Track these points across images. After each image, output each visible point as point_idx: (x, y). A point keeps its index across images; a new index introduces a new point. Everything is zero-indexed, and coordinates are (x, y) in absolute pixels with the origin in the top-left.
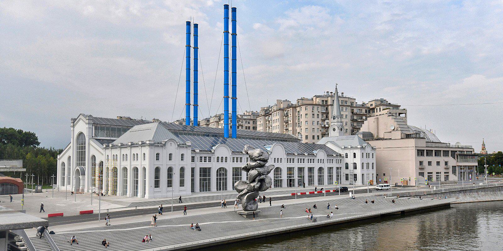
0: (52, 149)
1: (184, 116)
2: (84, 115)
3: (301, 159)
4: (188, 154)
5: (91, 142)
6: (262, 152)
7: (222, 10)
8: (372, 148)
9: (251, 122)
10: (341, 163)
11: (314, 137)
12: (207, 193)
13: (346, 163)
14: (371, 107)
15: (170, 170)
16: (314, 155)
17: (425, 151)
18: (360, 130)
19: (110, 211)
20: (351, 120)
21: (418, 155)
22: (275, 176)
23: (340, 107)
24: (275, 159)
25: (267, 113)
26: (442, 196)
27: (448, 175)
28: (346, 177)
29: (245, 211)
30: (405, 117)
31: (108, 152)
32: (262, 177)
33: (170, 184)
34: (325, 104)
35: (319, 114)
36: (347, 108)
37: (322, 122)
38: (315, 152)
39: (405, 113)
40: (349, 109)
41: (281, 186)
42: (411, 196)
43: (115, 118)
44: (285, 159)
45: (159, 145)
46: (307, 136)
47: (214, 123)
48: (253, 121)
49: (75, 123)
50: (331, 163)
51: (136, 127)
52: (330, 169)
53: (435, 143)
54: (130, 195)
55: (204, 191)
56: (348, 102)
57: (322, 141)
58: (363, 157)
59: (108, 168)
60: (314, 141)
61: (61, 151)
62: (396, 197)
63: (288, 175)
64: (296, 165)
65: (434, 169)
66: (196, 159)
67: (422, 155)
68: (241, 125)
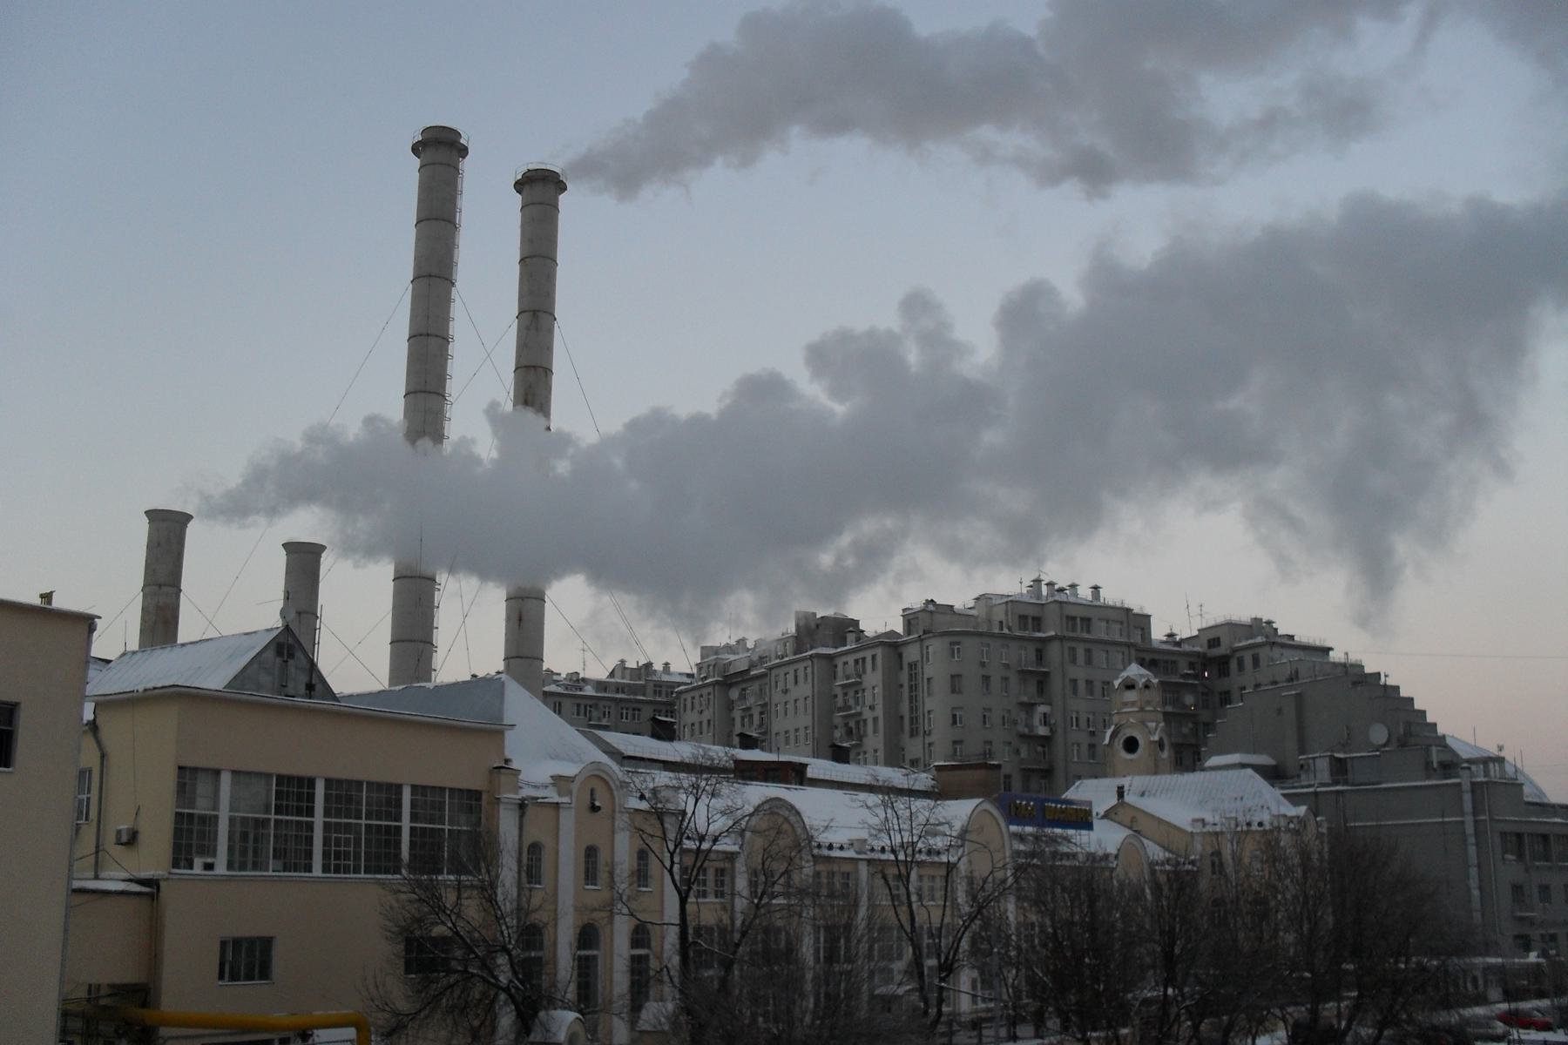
36: (988, 645)
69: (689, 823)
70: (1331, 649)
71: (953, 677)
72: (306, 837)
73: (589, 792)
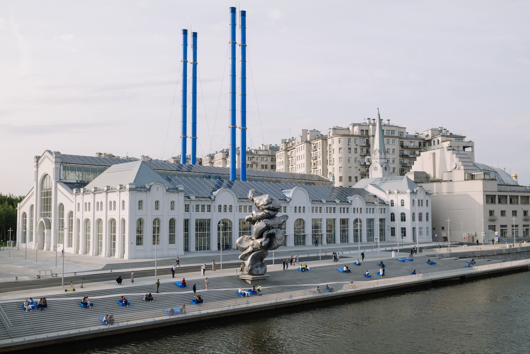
0: (11, 195)
1: (179, 152)
2: (50, 152)
3: (344, 208)
4: (179, 199)
5: (60, 187)
6: (271, 199)
7: (229, 15)
8: (426, 193)
9: (269, 159)
10: (384, 213)
11: (350, 178)
12: (204, 252)
13: (392, 213)
14: (427, 139)
15: (172, 222)
16: (348, 202)
17: (497, 197)
18: (411, 169)
19: (78, 274)
20: (400, 156)
21: (487, 202)
22: (342, 229)
23: (384, 138)
24: (296, 207)
25: (289, 146)
26: (518, 257)
27: (528, 229)
28: (392, 231)
30: (472, 152)
31: (79, 198)
32: (271, 231)
33: (155, 239)
34: (365, 135)
35: (357, 149)
38: (349, 198)
39: (472, 147)
40: (397, 140)
41: (304, 244)
42: (476, 256)
43: (95, 155)
44: (309, 208)
45: (142, 189)
46: (342, 177)
47: (220, 161)
48: (272, 157)
49: (39, 161)
50: (372, 213)
51: (114, 167)
53: (510, 185)
54: (105, 254)
55: (301, 245)
56: (395, 132)
57: (358, 186)
58: (413, 205)
59: (79, 220)
60: (350, 184)
61: (21, 199)
62: (455, 258)
63: (314, 230)
64: (324, 216)
65: (510, 220)
66: (191, 208)
67: (493, 202)
68: (254, 163)
69: (18, 243)
70: (465, 137)
71: (340, 177)
72: (241, 230)
73: (125, 209)
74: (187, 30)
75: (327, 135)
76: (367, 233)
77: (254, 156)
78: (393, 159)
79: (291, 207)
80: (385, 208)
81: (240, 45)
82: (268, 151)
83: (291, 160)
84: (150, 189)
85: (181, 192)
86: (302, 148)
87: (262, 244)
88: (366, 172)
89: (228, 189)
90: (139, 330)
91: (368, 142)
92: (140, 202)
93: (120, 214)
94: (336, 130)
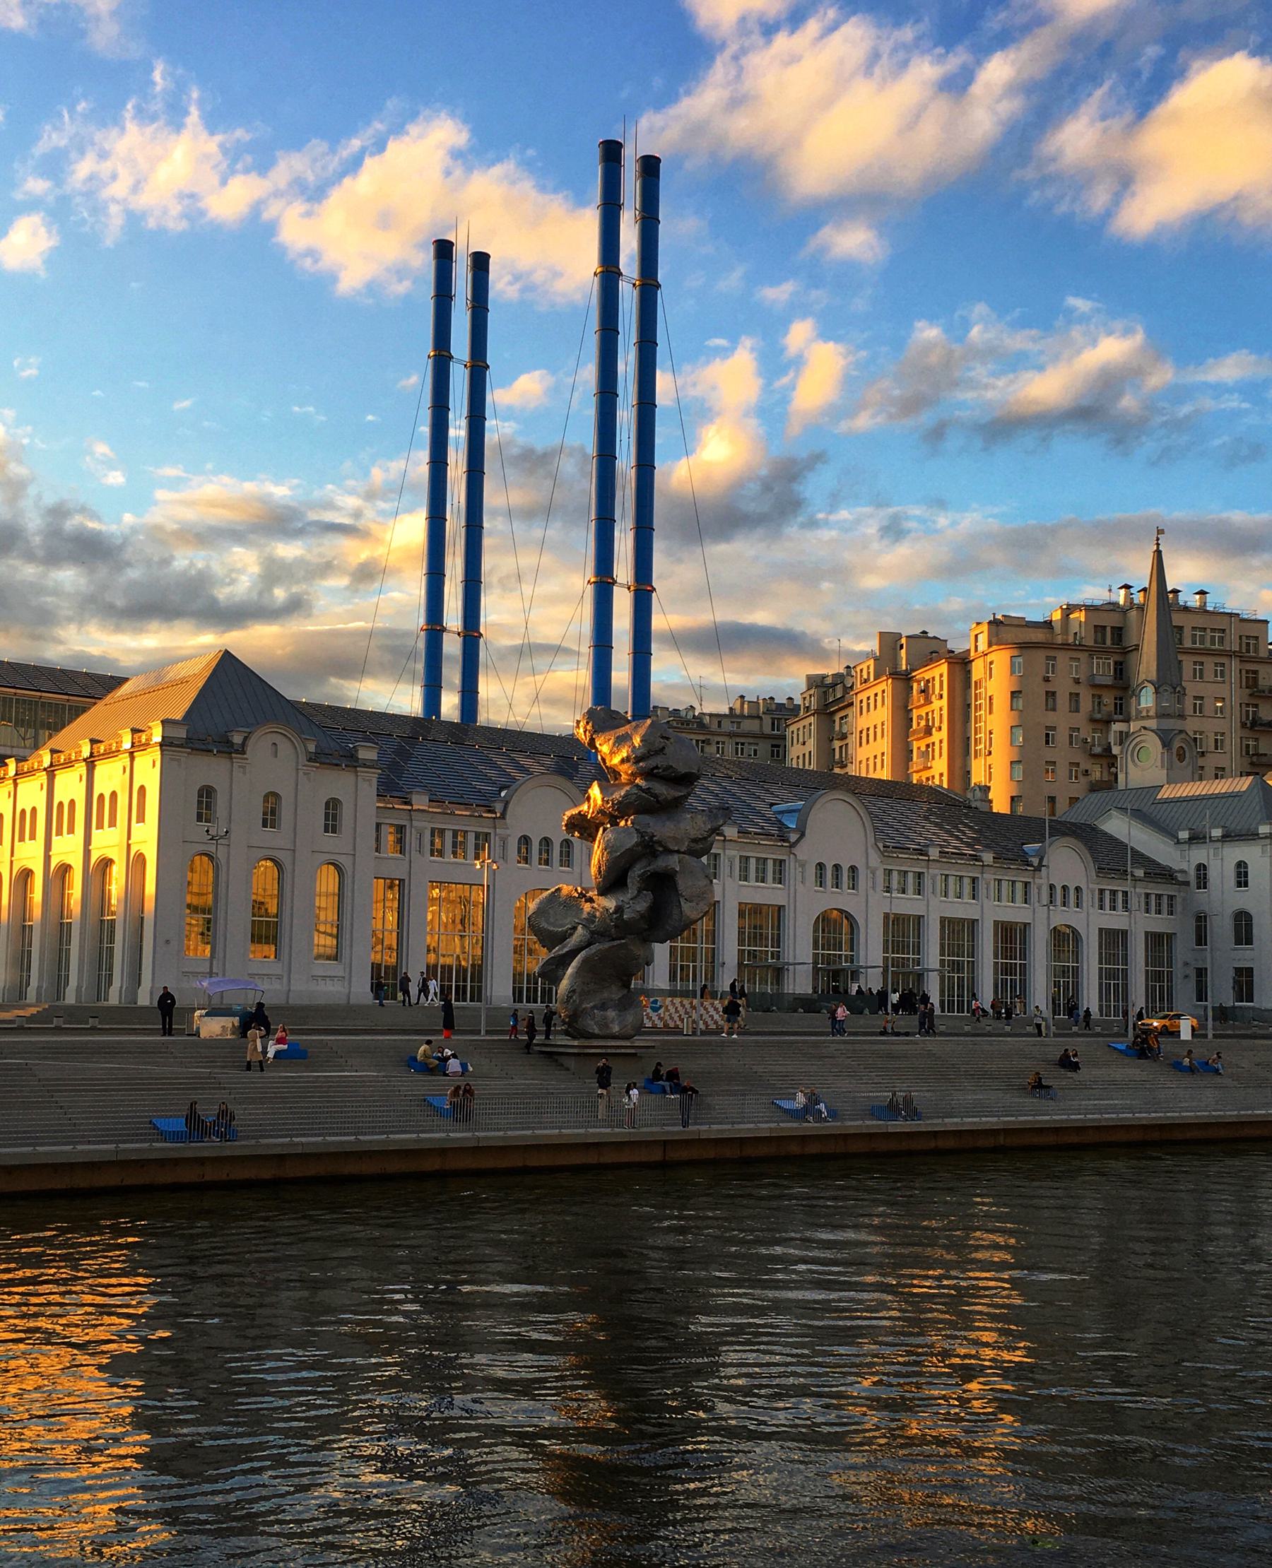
6: (663, 737)
9: (764, 748)
20: (1243, 725)
24: (821, 866)
29: (574, 1038)
35: (1078, 695)
37: (1094, 731)
48: (775, 742)
52: (1114, 941)
74: (452, 244)
75: (969, 651)
76: (1100, 984)
77: (708, 737)
78: (1216, 734)
79: (803, 865)
80: (1173, 894)
81: (634, 285)
82: (761, 718)
83: (841, 747)
84: (244, 744)
85: (365, 766)
86: (879, 698)
87: (623, 911)
88: (1110, 780)
89: (560, 781)
90: (59, 1187)
91: (1121, 670)
92: (206, 795)
93: (129, 838)
94: (1002, 628)
